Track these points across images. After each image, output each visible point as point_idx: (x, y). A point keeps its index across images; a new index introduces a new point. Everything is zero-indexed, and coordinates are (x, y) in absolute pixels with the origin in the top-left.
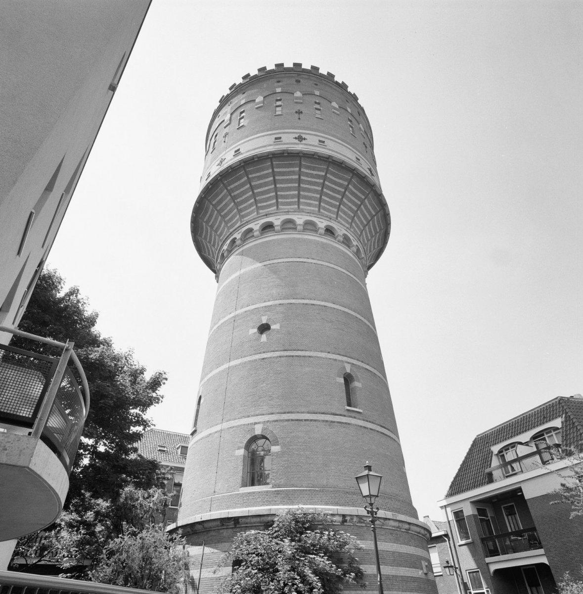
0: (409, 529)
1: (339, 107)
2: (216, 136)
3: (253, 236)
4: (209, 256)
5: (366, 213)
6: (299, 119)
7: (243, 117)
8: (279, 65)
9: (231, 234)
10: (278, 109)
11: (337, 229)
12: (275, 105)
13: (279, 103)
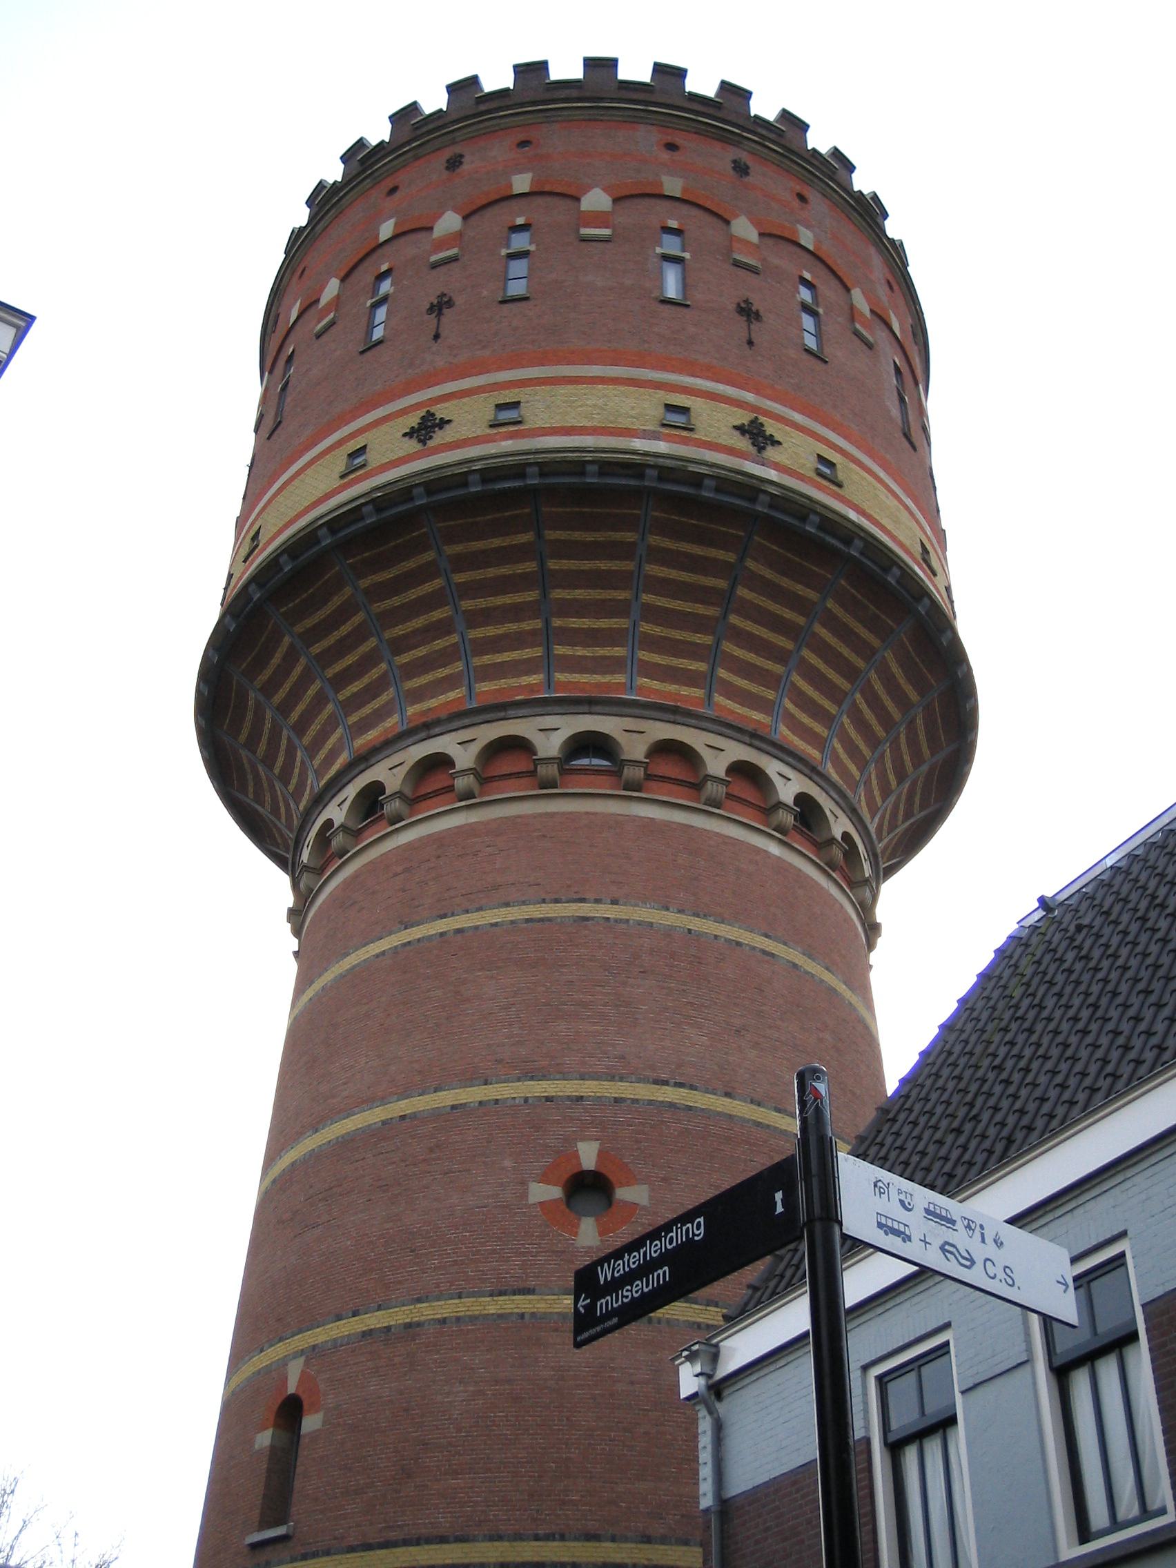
0: (556, 1353)
1: (761, 235)
2: (290, 359)
3: (450, 788)
4: (244, 753)
5: (673, 574)
6: (750, 343)
7: (384, 300)
8: (463, 89)
9: (363, 760)
10: (519, 268)
11: (828, 813)
12: (504, 252)
13: (520, 242)
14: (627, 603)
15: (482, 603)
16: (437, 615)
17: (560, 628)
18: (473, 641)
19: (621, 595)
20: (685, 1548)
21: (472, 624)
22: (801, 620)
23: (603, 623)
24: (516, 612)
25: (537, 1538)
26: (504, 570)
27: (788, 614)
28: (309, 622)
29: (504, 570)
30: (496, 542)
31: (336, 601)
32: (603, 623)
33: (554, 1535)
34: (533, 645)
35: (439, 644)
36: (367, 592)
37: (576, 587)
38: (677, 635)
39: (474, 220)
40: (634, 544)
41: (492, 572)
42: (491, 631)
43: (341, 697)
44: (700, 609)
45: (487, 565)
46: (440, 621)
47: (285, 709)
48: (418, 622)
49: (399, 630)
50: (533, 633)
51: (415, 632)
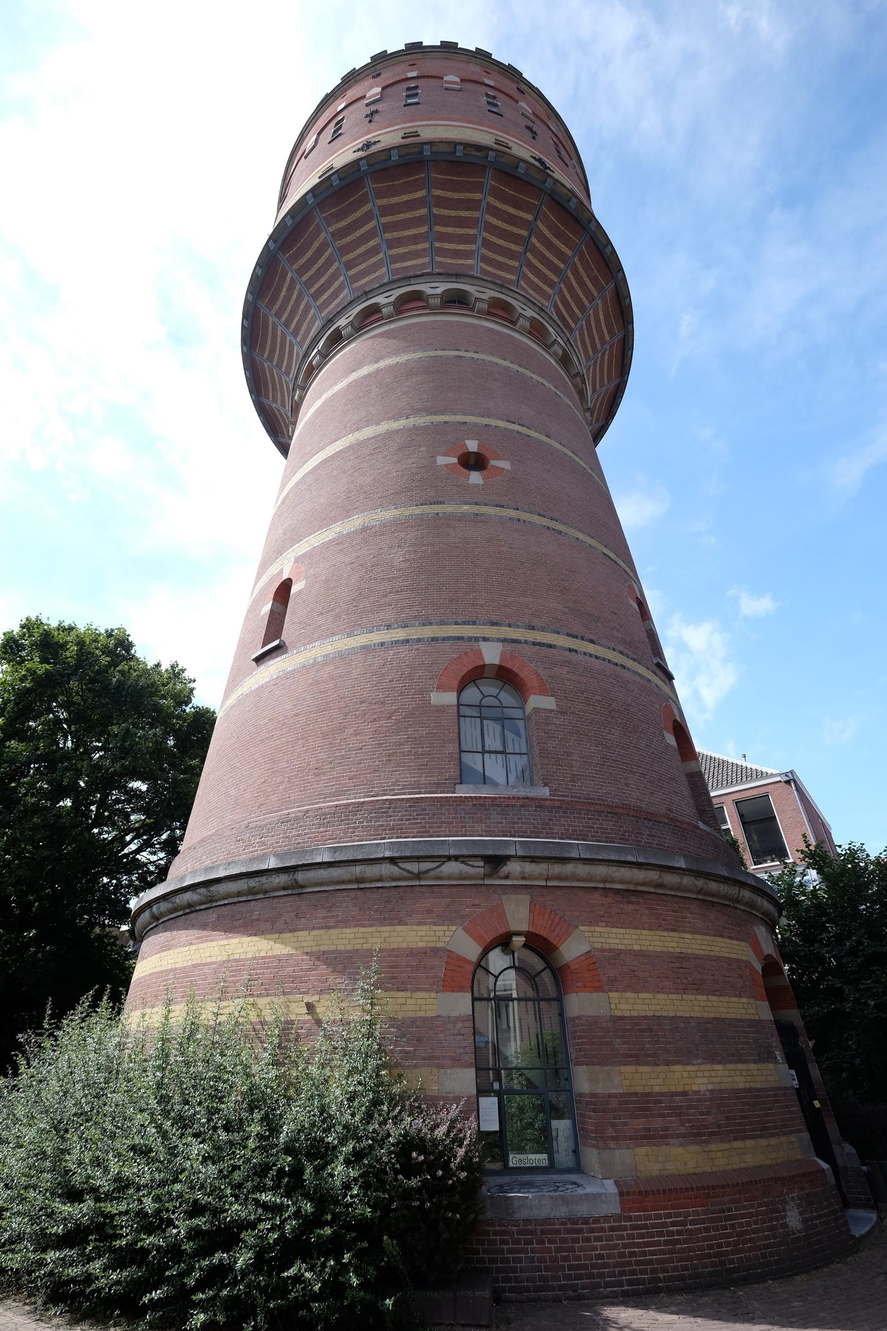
5: (499, 223)
14: (475, 236)
15: (396, 235)
16: (371, 243)
17: (438, 248)
18: (390, 256)
19: (472, 232)
20: (558, 635)
21: (390, 247)
22: (562, 266)
23: (461, 247)
24: (415, 239)
25: (456, 623)
26: (409, 215)
27: (556, 261)
28: (301, 262)
29: (409, 215)
30: (405, 198)
31: (316, 245)
32: (461, 247)
33: (469, 622)
34: (424, 257)
35: (373, 260)
36: (333, 234)
37: (448, 226)
38: (500, 259)
39: (388, 91)
40: (480, 201)
41: (402, 216)
42: (401, 250)
43: (318, 303)
44: (513, 247)
45: (400, 212)
46: (373, 247)
47: (287, 324)
48: (362, 250)
49: (351, 256)
50: (424, 250)
51: (360, 256)
